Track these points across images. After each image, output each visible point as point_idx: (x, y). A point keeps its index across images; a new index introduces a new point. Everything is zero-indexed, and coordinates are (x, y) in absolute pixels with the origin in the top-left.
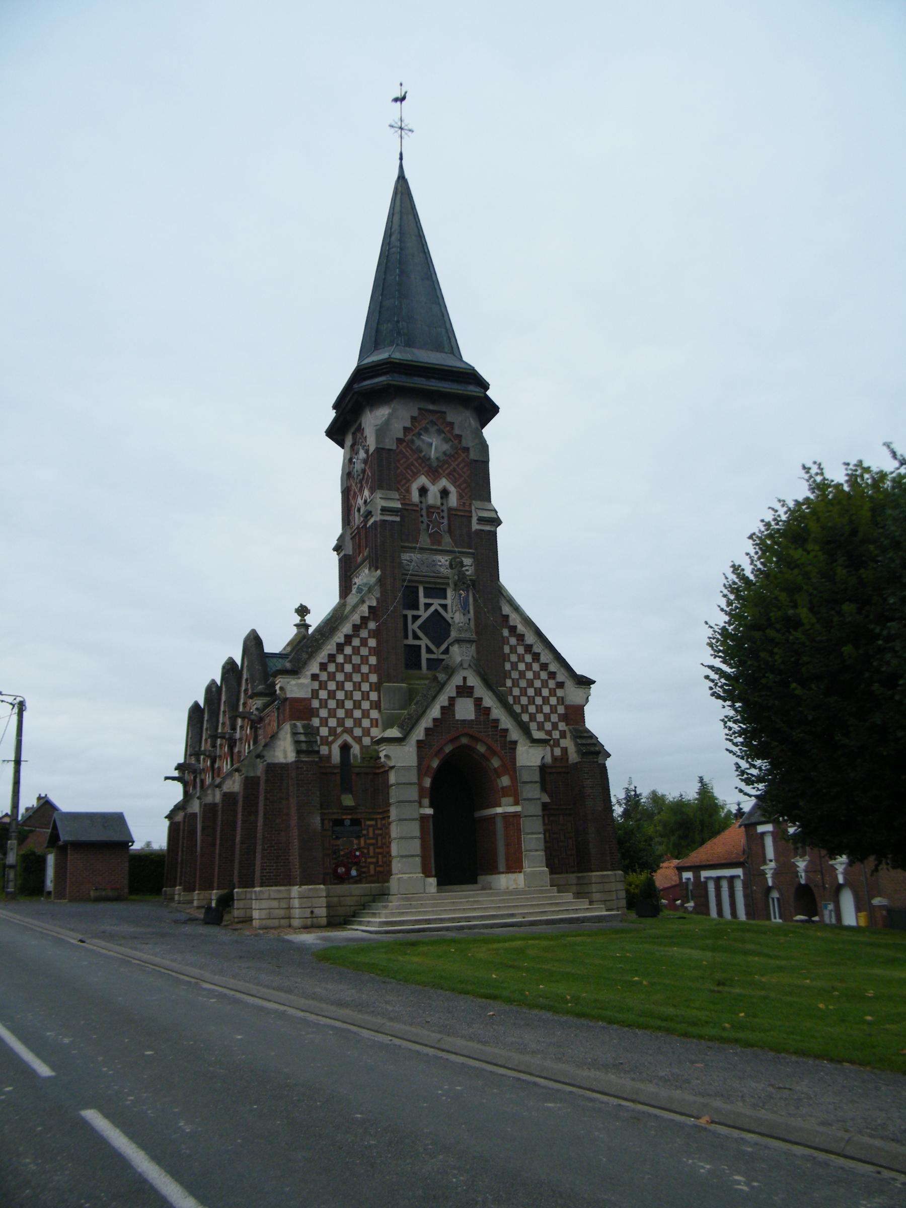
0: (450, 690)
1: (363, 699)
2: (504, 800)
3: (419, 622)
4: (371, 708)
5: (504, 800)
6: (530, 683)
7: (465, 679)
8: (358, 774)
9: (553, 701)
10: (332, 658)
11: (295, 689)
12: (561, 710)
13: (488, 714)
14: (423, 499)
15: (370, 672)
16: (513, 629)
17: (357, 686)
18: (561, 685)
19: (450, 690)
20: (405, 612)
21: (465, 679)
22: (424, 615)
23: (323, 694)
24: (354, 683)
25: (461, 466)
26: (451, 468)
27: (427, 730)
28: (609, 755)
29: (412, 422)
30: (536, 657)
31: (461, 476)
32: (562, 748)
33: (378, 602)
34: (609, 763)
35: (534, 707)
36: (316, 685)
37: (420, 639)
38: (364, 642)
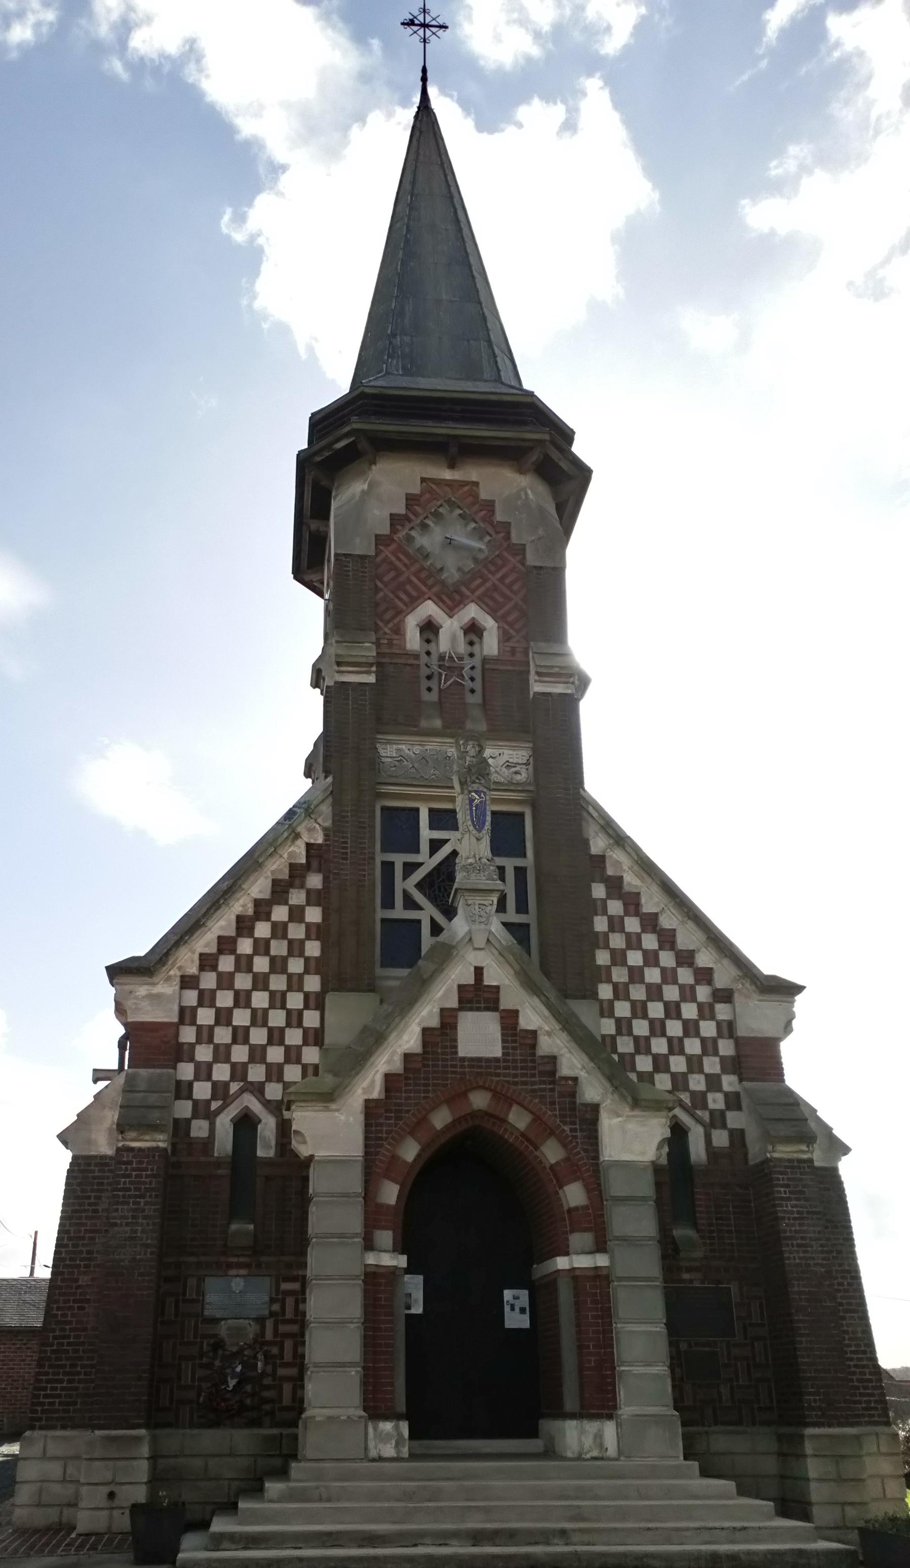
0: (442, 993)
1: (289, 1024)
2: (577, 1239)
3: (419, 875)
4: (309, 903)
5: (577, 1239)
6: (654, 992)
7: (479, 971)
8: (268, 1179)
9: (708, 1029)
10: (226, 945)
11: (145, 1004)
12: (726, 1048)
13: (534, 1046)
14: (432, 647)
16: (615, 886)
17: (278, 1000)
18: (725, 996)
19: (442, 993)
21: (479, 971)
22: (430, 863)
23: (206, 1016)
24: (272, 994)
25: (508, 581)
26: (488, 585)
27: (389, 1078)
28: (846, 1150)
30: (667, 939)
31: (509, 599)
32: (732, 1132)
33: (326, 836)
34: (846, 1167)
36: (191, 997)
37: (419, 908)
38: (297, 914)
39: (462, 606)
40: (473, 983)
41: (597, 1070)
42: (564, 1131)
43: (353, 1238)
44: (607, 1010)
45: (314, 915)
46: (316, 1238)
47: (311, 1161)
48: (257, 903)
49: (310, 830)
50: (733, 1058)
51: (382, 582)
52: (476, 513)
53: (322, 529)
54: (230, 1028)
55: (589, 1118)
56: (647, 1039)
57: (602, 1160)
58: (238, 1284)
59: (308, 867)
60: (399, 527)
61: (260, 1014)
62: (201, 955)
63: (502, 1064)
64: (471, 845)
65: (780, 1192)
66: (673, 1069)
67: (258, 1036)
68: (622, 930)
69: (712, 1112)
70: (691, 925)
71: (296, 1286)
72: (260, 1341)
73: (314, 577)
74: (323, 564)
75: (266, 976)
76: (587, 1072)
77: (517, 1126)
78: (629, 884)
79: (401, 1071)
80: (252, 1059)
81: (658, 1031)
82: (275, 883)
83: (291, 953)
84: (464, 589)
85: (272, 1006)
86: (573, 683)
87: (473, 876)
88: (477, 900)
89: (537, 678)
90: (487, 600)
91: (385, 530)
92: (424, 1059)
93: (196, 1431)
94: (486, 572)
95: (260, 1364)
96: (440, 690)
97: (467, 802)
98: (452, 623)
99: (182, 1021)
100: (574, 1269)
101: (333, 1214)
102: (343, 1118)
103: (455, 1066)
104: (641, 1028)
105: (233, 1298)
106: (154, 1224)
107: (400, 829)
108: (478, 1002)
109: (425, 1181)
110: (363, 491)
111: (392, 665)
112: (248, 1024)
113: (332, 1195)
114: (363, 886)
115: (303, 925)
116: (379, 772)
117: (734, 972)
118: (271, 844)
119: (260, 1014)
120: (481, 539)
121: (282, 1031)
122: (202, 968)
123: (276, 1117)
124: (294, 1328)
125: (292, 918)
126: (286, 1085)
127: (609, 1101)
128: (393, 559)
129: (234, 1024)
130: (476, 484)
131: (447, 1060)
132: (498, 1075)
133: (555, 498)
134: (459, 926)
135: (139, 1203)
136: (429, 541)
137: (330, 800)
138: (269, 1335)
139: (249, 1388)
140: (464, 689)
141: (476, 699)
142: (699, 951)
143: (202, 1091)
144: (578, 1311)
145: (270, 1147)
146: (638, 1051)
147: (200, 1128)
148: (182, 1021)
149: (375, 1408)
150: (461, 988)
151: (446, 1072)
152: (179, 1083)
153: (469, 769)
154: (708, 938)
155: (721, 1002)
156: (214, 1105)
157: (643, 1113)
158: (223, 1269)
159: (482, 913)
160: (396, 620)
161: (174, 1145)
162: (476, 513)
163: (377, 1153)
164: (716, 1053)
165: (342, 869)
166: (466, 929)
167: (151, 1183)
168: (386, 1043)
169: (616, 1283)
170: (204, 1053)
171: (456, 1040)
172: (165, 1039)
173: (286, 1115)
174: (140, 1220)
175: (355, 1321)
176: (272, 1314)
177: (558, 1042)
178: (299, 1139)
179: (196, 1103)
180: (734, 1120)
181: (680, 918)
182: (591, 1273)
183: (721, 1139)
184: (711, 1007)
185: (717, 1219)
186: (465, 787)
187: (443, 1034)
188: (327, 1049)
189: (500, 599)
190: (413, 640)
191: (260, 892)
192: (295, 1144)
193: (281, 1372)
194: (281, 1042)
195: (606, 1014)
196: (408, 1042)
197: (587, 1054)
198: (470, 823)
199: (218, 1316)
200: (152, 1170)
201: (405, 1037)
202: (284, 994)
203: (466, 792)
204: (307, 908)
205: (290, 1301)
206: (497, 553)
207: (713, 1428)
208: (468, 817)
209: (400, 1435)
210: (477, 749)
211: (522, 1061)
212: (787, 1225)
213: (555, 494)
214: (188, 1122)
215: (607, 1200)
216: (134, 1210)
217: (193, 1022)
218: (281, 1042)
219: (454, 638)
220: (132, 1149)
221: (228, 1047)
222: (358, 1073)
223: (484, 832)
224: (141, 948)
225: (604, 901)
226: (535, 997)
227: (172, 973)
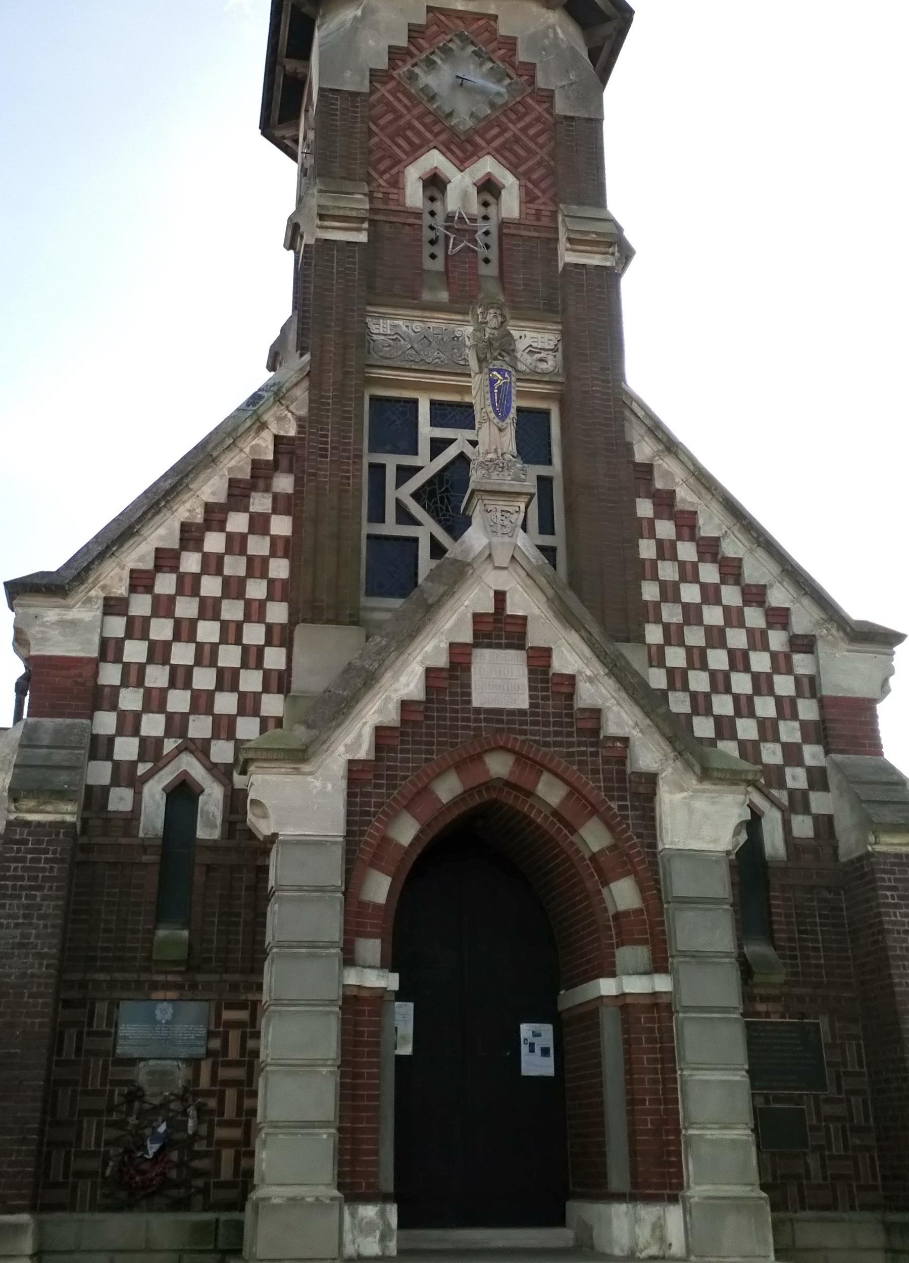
0: (453, 623)
1: (245, 665)
2: (631, 955)
4: (275, 511)
6: (716, 638)
7: (500, 597)
8: (209, 868)
9: (784, 685)
10: (166, 560)
11: (54, 633)
12: (808, 710)
13: (570, 696)
14: (437, 206)
15: (270, 597)
16: (665, 502)
17: (232, 633)
18: (804, 644)
19: (453, 623)
21: (500, 597)
22: (431, 468)
24: (225, 625)
25: (531, 132)
26: (508, 135)
27: (380, 732)
30: (731, 570)
32: (817, 818)
33: (300, 427)
35: (728, 699)
36: (117, 626)
37: (416, 522)
38: (259, 524)
39: (475, 158)
40: (492, 611)
41: (654, 729)
42: (610, 808)
43: (327, 948)
44: (657, 658)
45: (281, 526)
46: (277, 947)
47: (273, 842)
48: (209, 508)
49: (280, 419)
50: (815, 723)
51: (377, 125)
52: (494, 51)
53: (300, 70)
54: (167, 668)
55: (646, 788)
56: (707, 696)
57: (660, 848)
58: (164, 1012)
59: (275, 466)
60: (400, 63)
61: (207, 649)
62: (132, 571)
63: (529, 718)
64: (492, 440)
65: (886, 897)
66: (741, 735)
67: (204, 679)
68: (674, 557)
69: (792, 793)
70: (760, 553)
71: (242, 1015)
72: (190, 1091)
73: (288, 133)
74: (298, 117)
75: (217, 602)
76: (641, 731)
77: (548, 800)
78: (683, 500)
79: (397, 724)
80: (195, 709)
81: (721, 687)
82: (233, 483)
83: (250, 574)
84: (478, 140)
85: (224, 640)
86: (613, 254)
87: (494, 475)
88: (501, 504)
89: (569, 246)
90: (507, 154)
91: (382, 63)
92: (403, 734)
93: (98, 1216)
94: (505, 121)
95: (191, 1123)
96: (447, 256)
97: (487, 383)
98: (463, 177)
99: (103, 656)
100: (624, 995)
101: (301, 916)
102: (318, 784)
103: (468, 719)
104: (699, 681)
105: (158, 1033)
106: (53, 926)
107: (394, 423)
108: (499, 637)
109: (423, 872)
110: (355, 17)
111: (389, 224)
112: (191, 663)
113: (300, 889)
114: (347, 491)
115: (268, 539)
116: (369, 352)
117: (817, 614)
118: (229, 434)
119: (207, 649)
120: (499, 81)
121: (235, 672)
122: (133, 589)
123: (224, 785)
124: (239, 1073)
125: (252, 529)
126: (239, 745)
127: (670, 770)
128: (391, 98)
129: (172, 662)
130: (495, 18)
131: (457, 711)
132: (524, 732)
133: (587, 44)
134: (475, 538)
135: (35, 897)
136: (438, 80)
137: (306, 383)
138: (205, 1081)
139: (174, 1156)
140: (476, 257)
141: (492, 270)
142: (772, 586)
143: (126, 749)
144: (628, 1052)
145: (214, 826)
146: (696, 711)
147: (121, 799)
148: (103, 656)
149: (353, 1188)
150: (478, 618)
151: (457, 727)
152: (95, 738)
153: (490, 343)
154: (783, 571)
155: (800, 652)
157: (714, 787)
158: (144, 990)
159: (506, 522)
160: (394, 171)
161: (84, 821)
162: (494, 51)
163: (362, 833)
164: (794, 716)
165: (319, 469)
166: (485, 541)
167: (51, 869)
168: (378, 685)
169: (681, 1015)
170: (131, 700)
171: (469, 686)
172: (79, 680)
173: (238, 780)
174: (35, 921)
175: (330, 1062)
176: (209, 1053)
177: (603, 691)
178: (258, 811)
179: (117, 765)
180: (820, 802)
181: (747, 543)
182: (648, 1001)
183: (803, 827)
184: (788, 658)
185: (800, 932)
186: (484, 364)
187: (452, 677)
188: (294, 697)
189: (522, 153)
190: (414, 194)
191: (213, 493)
192: (251, 818)
193: (221, 1133)
194: (192, 638)
195: (654, 663)
196: (408, 685)
197: (642, 708)
198: (490, 409)
199: (135, 1056)
200: (54, 852)
201: (403, 679)
202: (239, 626)
203: (486, 370)
204: (273, 517)
205: (234, 1036)
206: (518, 99)
207: (798, 1215)
208: (489, 402)
209: (387, 1225)
210: (500, 319)
211: (555, 715)
212: (895, 940)
213: (588, 40)
214: (105, 790)
215: (668, 902)
216: (27, 907)
217: (118, 659)
218: (234, 688)
219: (465, 195)
220: (28, 824)
221: (163, 692)
222: (339, 725)
223: (508, 420)
224: (52, 558)
225: (651, 522)
226: (573, 632)
227: (93, 593)
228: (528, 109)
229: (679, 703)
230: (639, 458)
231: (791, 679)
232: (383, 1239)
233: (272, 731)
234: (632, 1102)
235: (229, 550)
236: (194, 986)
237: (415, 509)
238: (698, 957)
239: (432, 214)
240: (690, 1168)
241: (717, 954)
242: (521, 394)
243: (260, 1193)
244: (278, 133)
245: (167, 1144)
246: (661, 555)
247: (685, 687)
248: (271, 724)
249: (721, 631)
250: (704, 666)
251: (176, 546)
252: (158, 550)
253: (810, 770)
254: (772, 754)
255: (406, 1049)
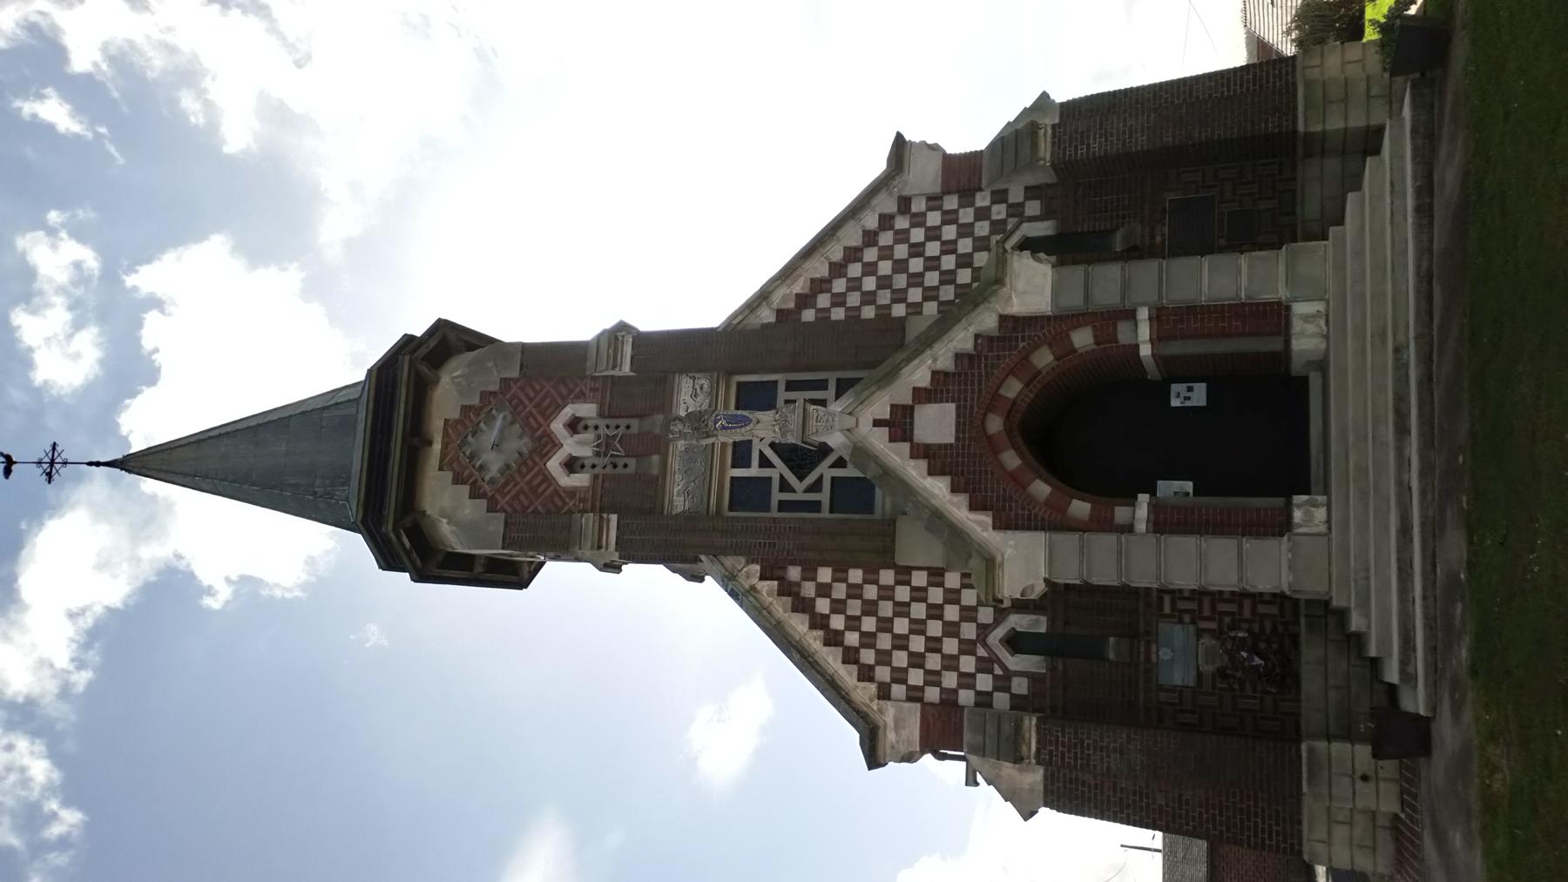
0: (897, 457)
2: (1123, 334)
3: (791, 478)
4: (814, 579)
7: (877, 423)
9: (934, 219)
10: (850, 657)
11: (904, 733)
12: (951, 202)
13: (946, 374)
14: (588, 463)
16: (804, 301)
17: (902, 609)
18: (904, 203)
19: (897, 457)
20: (774, 504)
21: (877, 423)
22: (780, 468)
23: (916, 677)
24: (896, 614)
25: (532, 394)
27: (973, 507)
28: (1044, 96)
29: (463, 483)
30: (853, 254)
32: (1027, 198)
33: (754, 561)
36: (898, 690)
37: (771, 465)
38: (824, 590)
44: (916, 309)
45: (825, 575)
48: (813, 626)
49: (748, 577)
55: (1012, 324)
56: (942, 273)
64: (764, 429)
67: (935, 628)
68: (844, 295)
69: (1009, 215)
70: (840, 234)
72: (1218, 634)
73: (526, 569)
75: (880, 620)
80: (956, 635)
82: (795, 610)
83: (859, 597)
85: (907, 615)
88: (812, 422)
91: (483, 503)
93: (1303, 697)
95: (1241, 635)
99: (920, 700)
101: (1100, 562)
102: (1009, 551)
104: (932, 279)
105: (1179, 658)
107: (749, 494)
111: (602, 499)
113: (1081, 562)
120: (494, 418)
126: (980, 603)
132: (972, 408)
134: (835, 440)
136: (494, 463)
137: (722, 558)
138: (1213, 625)
139: (1262, 645)
141: (635, 423)
143: (984, 682)
145: (1037, 621)
146: (953, 282)
148: (920, 700)
149: (1282, 526)
150: (892, 440)
152: (977, 704)
156: (998, 671)
161: (1034, 711)
163: (1043, 519)
164: (956, 212)
170: (950, 680)
173: (1007, 604)
176: (1193, 622)
179: (996, 689)
180: (1016, 195)
183: (1033, 208)
184: (915, 215)
190: (580, 480)
192: (1033, 596)
194: (906, 637)
202: (897, 604)
205: (1181, 605)
213: (459, 352)
214: (1013, 696)
217: (922, 689)
218: (940, 607)
219: (580, 443)
220: (1038, 750)
224: (851, 736)
228: (514, 396)
229: (948, 293)
230: (772, 319)
231: (929, 214)
232: (1316, 505)
233: (973, 580)
234: (1225, 335)
235: (842, 612)
236: (1148, 633)
237: (811, 479)
238: (1126, 286)
239: (594, 466)
240: (1268, 297)
241: (1123, 276)
242: (726, 407)
243: (1286, 589)
244: (526, 576)
245: (1254, 651)
246: (842, 304)
247: (936, 288)
248: (966, 581)
249: (896, 262)
250: (921, 275)
251: (840, 649)
252: (844, 662)
253: (993, 202)
254: (982, 229)
255: (1188, 486)
